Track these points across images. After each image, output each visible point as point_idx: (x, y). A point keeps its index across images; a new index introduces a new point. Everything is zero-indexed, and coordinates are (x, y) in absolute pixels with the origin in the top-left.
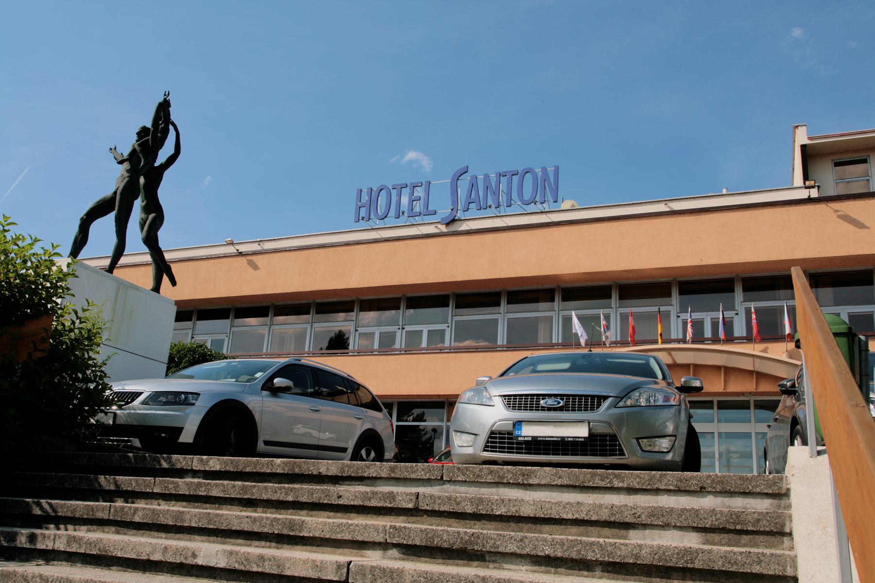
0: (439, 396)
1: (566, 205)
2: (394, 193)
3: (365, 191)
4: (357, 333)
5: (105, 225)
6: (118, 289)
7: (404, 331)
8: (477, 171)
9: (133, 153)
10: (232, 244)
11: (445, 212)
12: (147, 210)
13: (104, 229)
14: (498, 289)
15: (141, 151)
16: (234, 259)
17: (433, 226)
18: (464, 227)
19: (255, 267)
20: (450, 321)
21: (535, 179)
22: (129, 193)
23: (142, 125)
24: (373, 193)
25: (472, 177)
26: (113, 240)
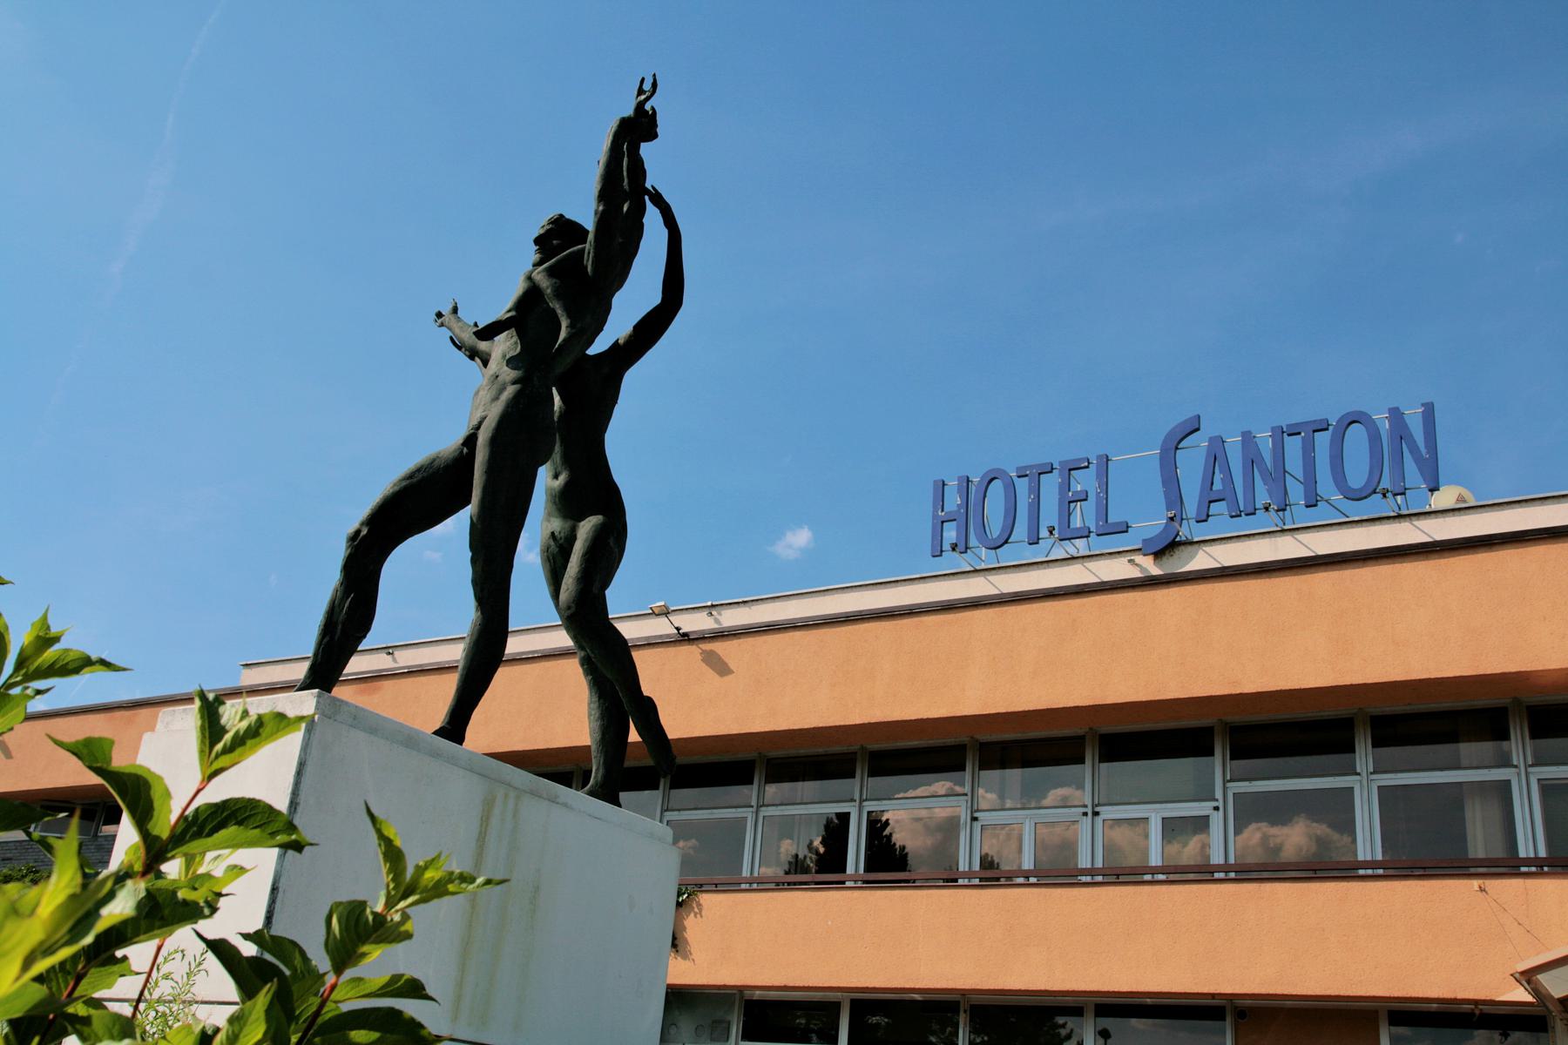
0: (1213, 996)
1: (1445, 498)
2: (1022, 486)
3: (953, 484)
4: (977, 826)
5: (435, 561)
6: (488, 804)
7: (1099, 820)
8: (1225, 425)
9: (530, 300)
10: (666, 613)
11: (1151, 524)
12: (570, 504)
13: (431, 574)
14: (1341, 711)
15: (558, 294)
16: (672, 650)
17: (1124, 560)
18: (1201, 560)
19: (722, 669)
20: (1219, 794)
21: (1374, 437)
22: (518, 439)
23: (552, 213)
24: (973, 489)
25: (1211, 440)
26: (464, 615)
